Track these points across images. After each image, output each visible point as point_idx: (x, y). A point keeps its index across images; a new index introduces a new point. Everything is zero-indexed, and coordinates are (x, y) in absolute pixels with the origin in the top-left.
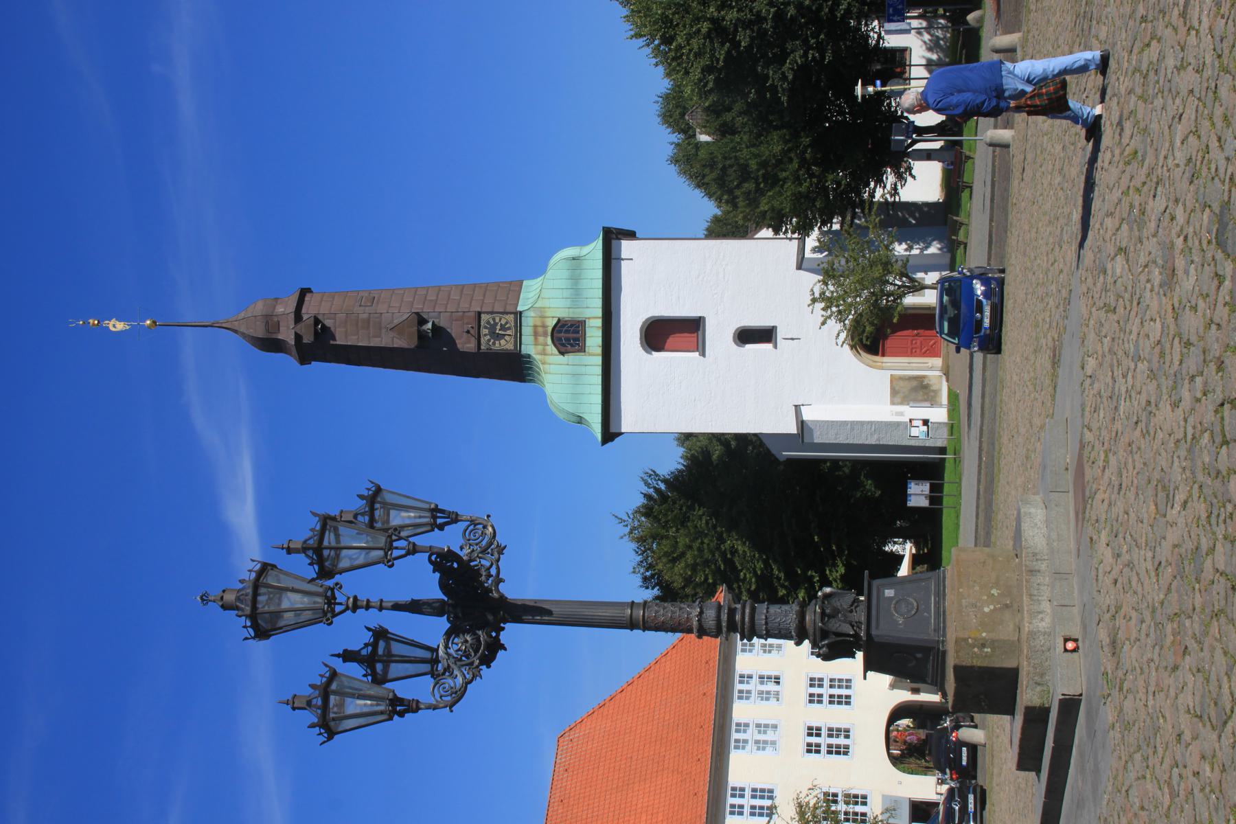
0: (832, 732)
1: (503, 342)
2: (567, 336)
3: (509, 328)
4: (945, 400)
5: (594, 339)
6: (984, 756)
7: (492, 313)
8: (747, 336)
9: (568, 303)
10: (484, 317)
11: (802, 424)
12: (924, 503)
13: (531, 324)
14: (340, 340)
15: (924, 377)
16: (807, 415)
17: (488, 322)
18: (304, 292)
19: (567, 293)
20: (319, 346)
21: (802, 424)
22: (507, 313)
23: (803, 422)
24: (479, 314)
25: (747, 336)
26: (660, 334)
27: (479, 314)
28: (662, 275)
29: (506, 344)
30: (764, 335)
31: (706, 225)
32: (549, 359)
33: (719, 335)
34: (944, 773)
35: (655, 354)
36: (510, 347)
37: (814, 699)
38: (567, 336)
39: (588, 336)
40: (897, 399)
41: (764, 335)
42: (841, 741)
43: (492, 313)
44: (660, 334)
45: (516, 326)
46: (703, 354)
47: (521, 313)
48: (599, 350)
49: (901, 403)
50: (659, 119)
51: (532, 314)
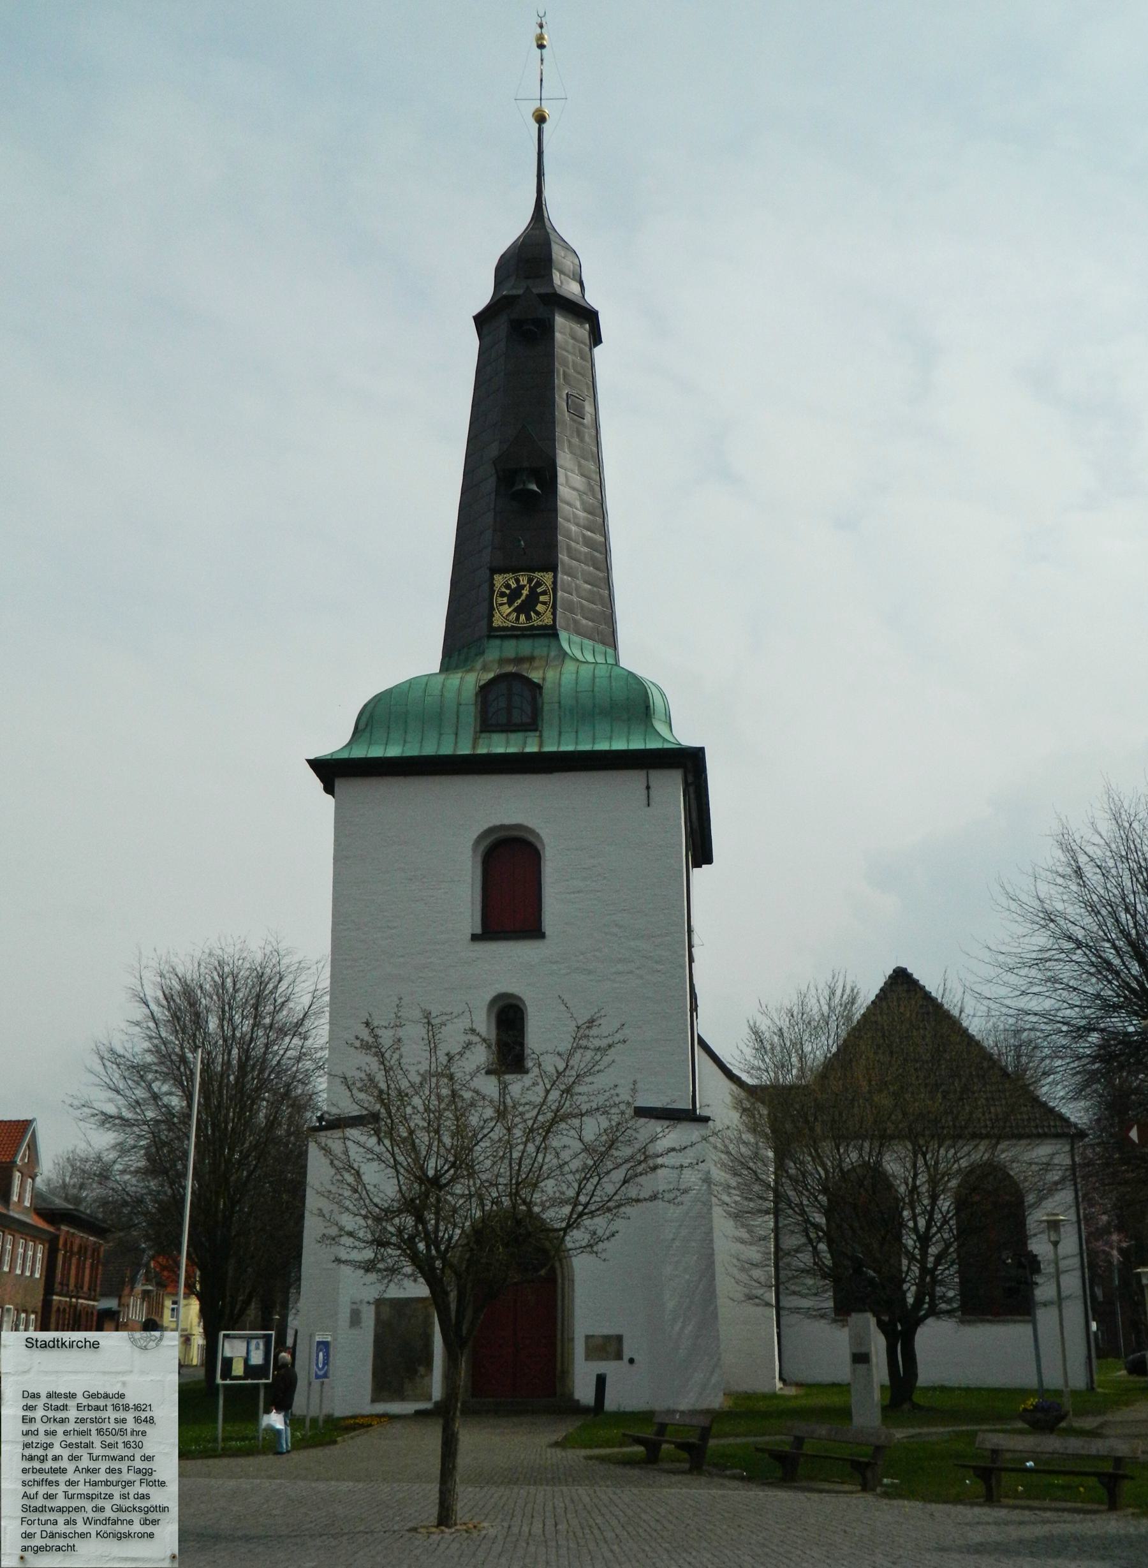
3: (529, 618)
5: (500, 745)
8: (509, 1016)
13: (537, 653)
25: (509, 1016)
33: (509, 966)
40: (386, 1310)
45: (532, 628)
47: (555, 636)
48: (481, 750)
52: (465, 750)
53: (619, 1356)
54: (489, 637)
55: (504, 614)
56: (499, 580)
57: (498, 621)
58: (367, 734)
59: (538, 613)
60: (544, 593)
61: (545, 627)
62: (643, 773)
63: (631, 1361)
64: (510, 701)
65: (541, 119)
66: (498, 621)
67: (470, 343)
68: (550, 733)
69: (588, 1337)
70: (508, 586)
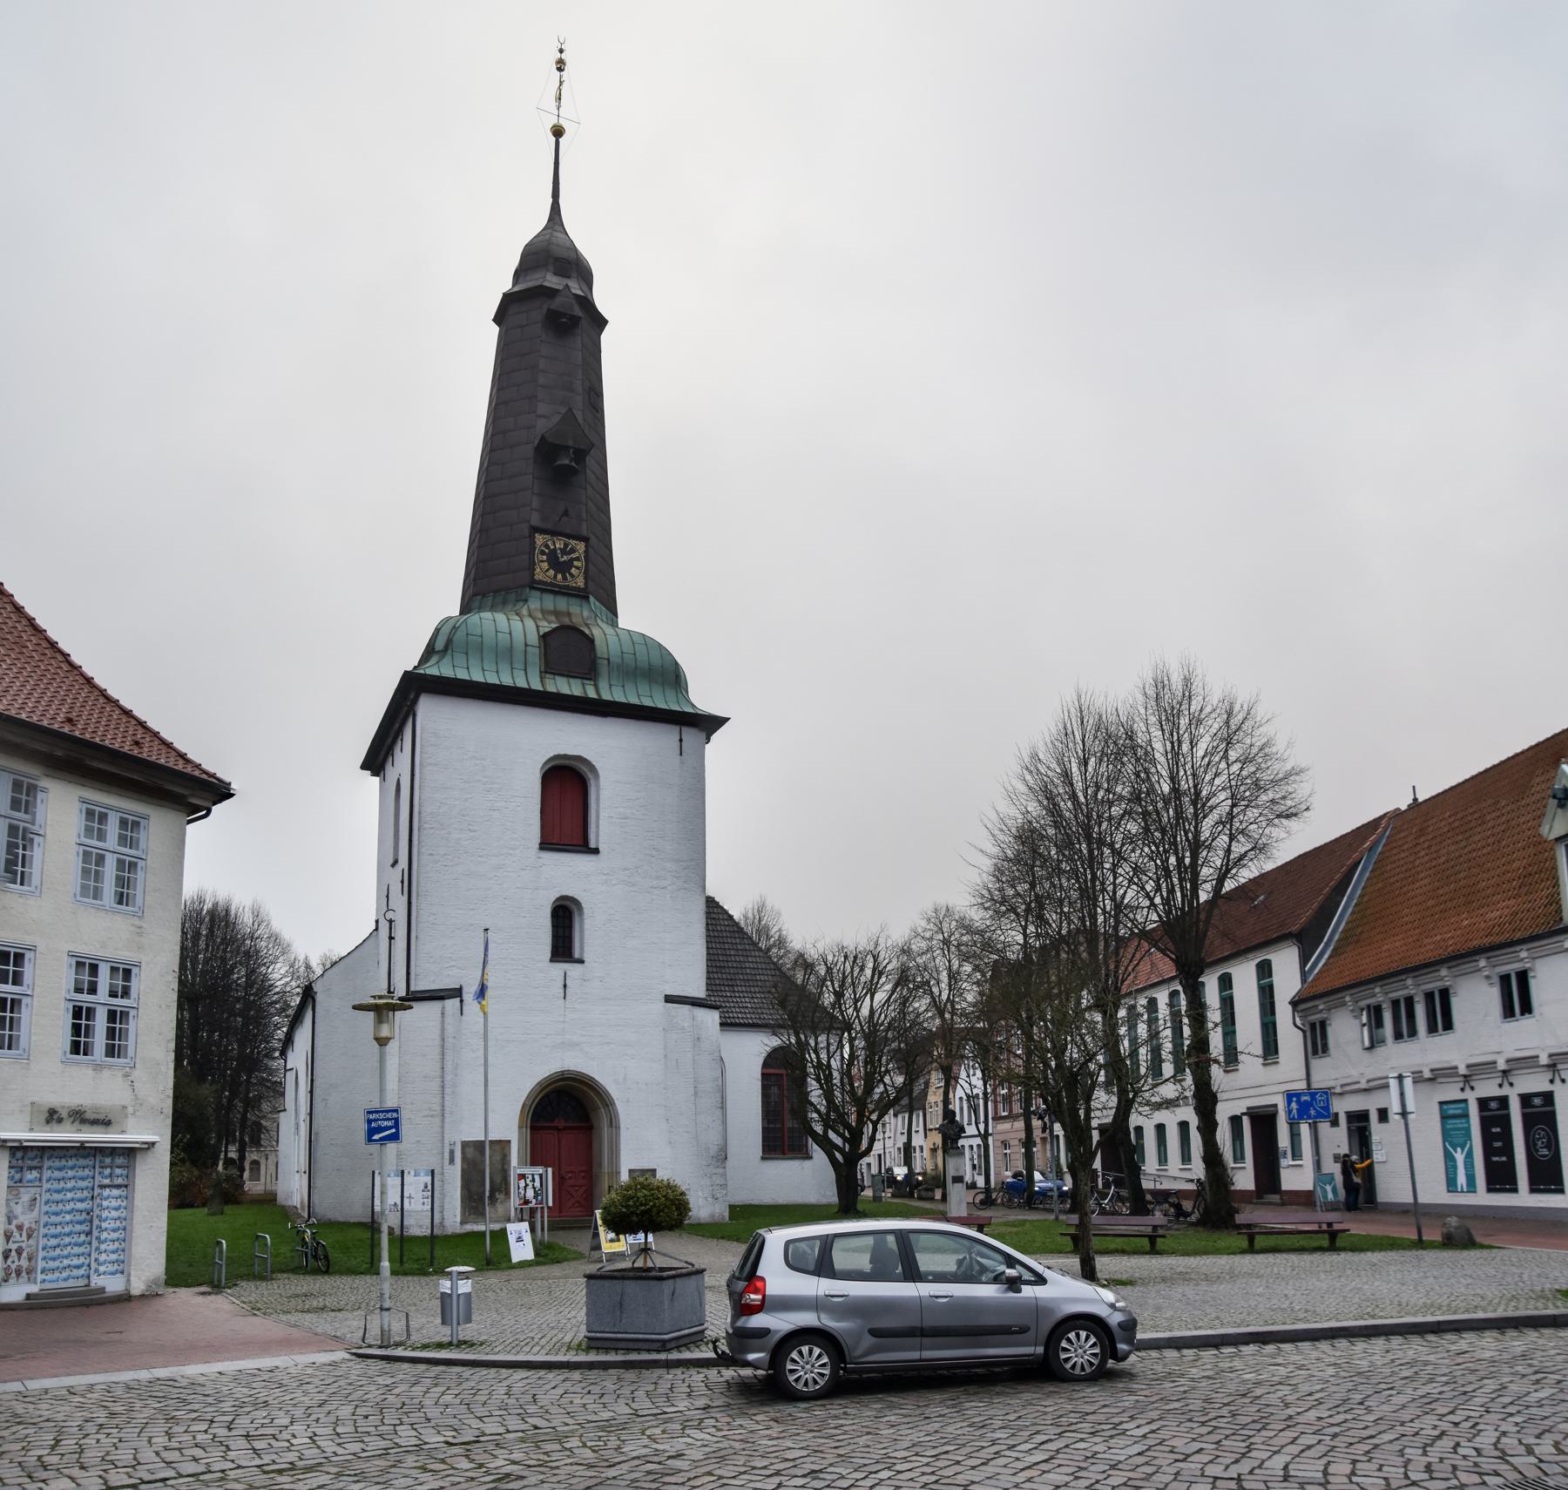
0: (127, 868)
1: (545, 566)
3: (565, 578)
4: (469, 1227)
8: (564, 915)
9: (615, 660)
10: (581, 547)
12: (515, 1259)
15: (507, 1193)
17: (573, 550)
19: (629, 658)
23: (593, 1344)
25: (564, 915)
26: (566, 785)
27: (585, 540)
30: (563, 947)
31: (1214, 688)
32: (530, 623)
33: (566, 873)
37: (87, 968)
40: (470, 1152)
41: (563, 947)
42: (99, 1040)
44: (566, 785)
45: (567, 587)
48: (551, 688)
49: (464, 1159)
50: (1120, 692)
51: (586, 614)
52: (536, 685)
54: (532, 588)
55: (543, 572)
56: (540, 539)
57: (539, 576)
58: (448, 657)
60: (578, 559)
61: (579, 589)
62: (677, 728)
64: (570, 650)
65: (558, 132)
66: (539, 576)
68: (603, 685)
70: (547, 546)
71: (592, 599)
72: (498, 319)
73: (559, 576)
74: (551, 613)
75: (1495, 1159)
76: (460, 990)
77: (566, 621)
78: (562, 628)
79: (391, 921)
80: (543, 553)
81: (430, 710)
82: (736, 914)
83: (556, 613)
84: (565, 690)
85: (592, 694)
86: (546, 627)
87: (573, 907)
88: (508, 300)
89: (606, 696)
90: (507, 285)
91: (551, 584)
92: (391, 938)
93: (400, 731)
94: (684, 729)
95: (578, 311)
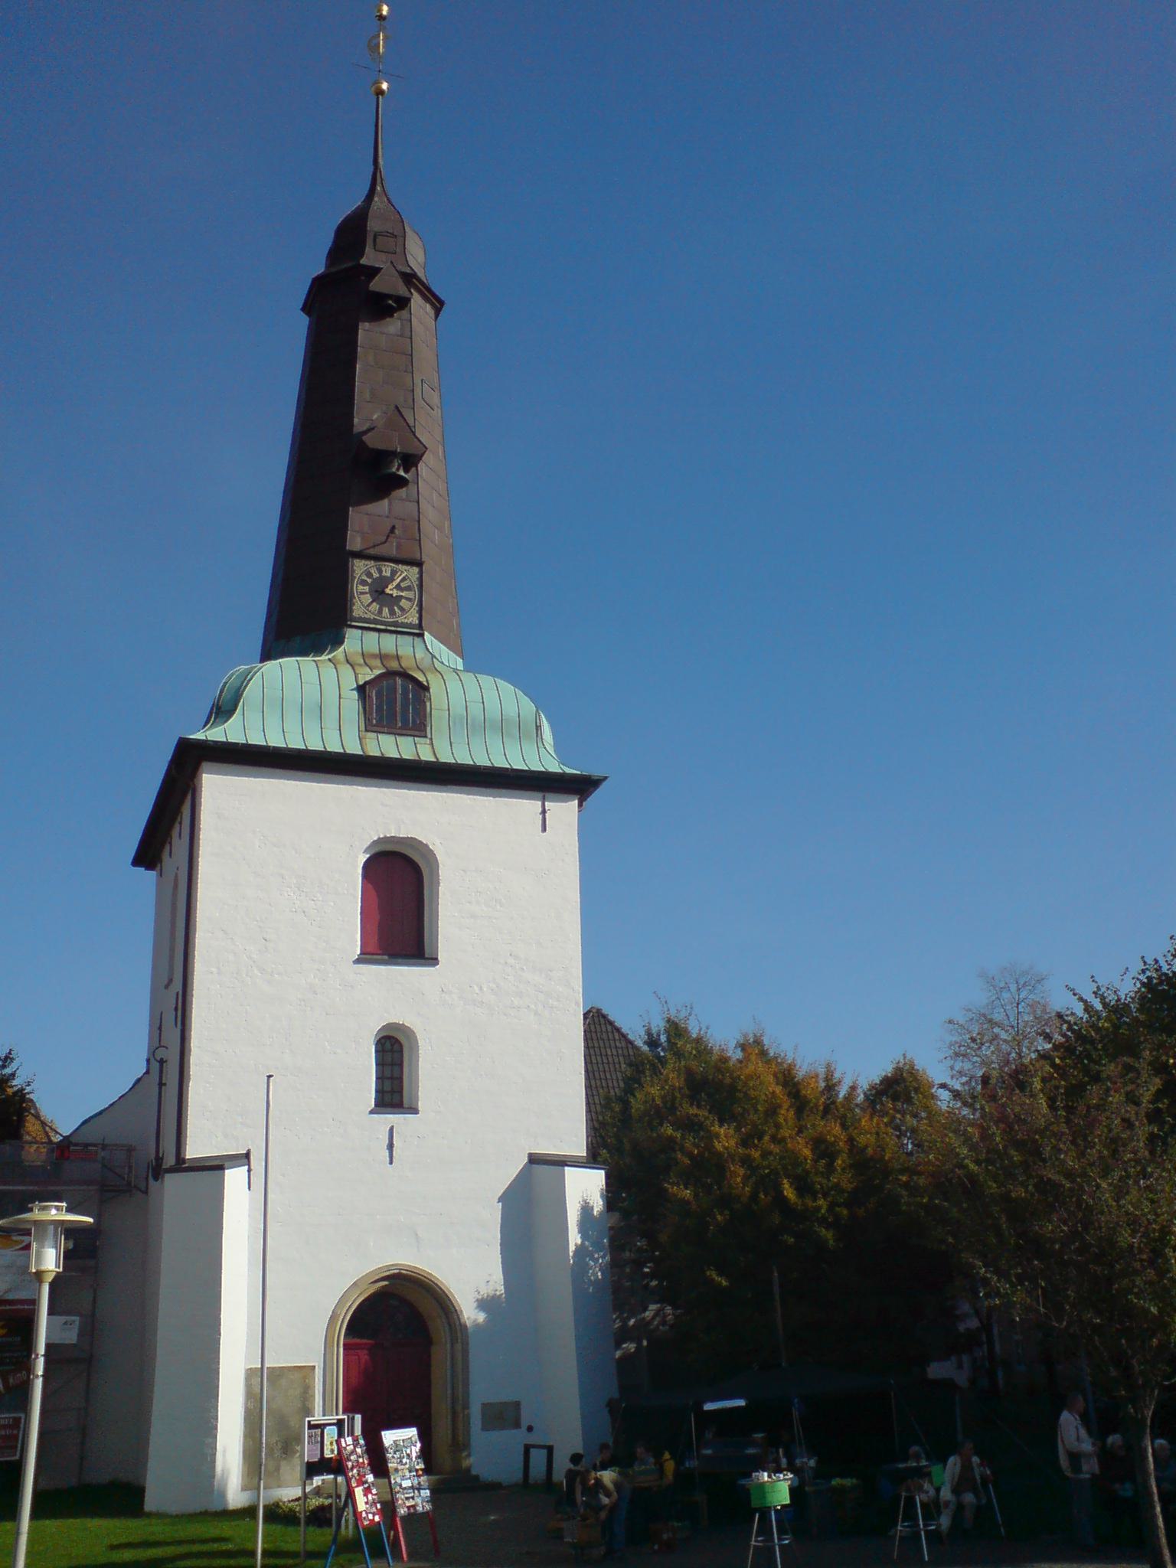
1: (368, 599)
2: (395, 699)
3: (392, 613)
6: (249, 1323)
7: (421, 586)
8: (393, 1053)
11: (215, 1167)
12: (389, 1437)
14: (366, 332)
16: (235, 1178)
18: (438, 304)
20: (350, 294)
21: (215, 1167)
22: (420, 612)
23: (221, 1168)
24: (419, 564)
25: (393, 1053)
27: (419, 564)
28: (514, 880)
29: (362, 603)
30: (393, 1090)
33: (395, 992)
34: (672, 1326)
35: (363, 858)
36: (358, 610)
38: (395, 699)
39: (393, 743)
41: (393, 1090)
43: (421, 586)
45: (396, 624)
46: (358, 961)
47: (421, 635)
48: (373, 751)
52: (354, 748)
53: (517, 1425)
59: (402, 609)
62: (540, 795)
63: (530, 1429)
67: (304, 321)
69: (486, 1407)
70: (369, 575)
71: (427, 635)
72: (307, 308)
73: (386, 610)
74: (374, 656)
75: (709, 1406)
76: (247, 1155)
77: (394, 665)
78: (390, 674)
79: (162, 1062)
80: (363, 583)
81: (216, 787)
82: (637, 1036)
83: (382, 657)
84: (392, 753)
85: (426, 755)
86: (367, 675)
87: (402, 1039)
88: (318, 283)
89: (446, 758)
90: (320, 269)
91: (375, 622)
92: (161, 1084)
93: (178, 811)
94: (548, 795)
95: (402, 290)
